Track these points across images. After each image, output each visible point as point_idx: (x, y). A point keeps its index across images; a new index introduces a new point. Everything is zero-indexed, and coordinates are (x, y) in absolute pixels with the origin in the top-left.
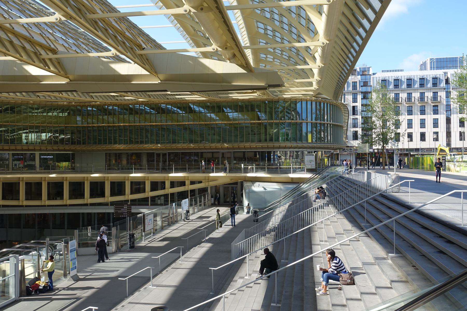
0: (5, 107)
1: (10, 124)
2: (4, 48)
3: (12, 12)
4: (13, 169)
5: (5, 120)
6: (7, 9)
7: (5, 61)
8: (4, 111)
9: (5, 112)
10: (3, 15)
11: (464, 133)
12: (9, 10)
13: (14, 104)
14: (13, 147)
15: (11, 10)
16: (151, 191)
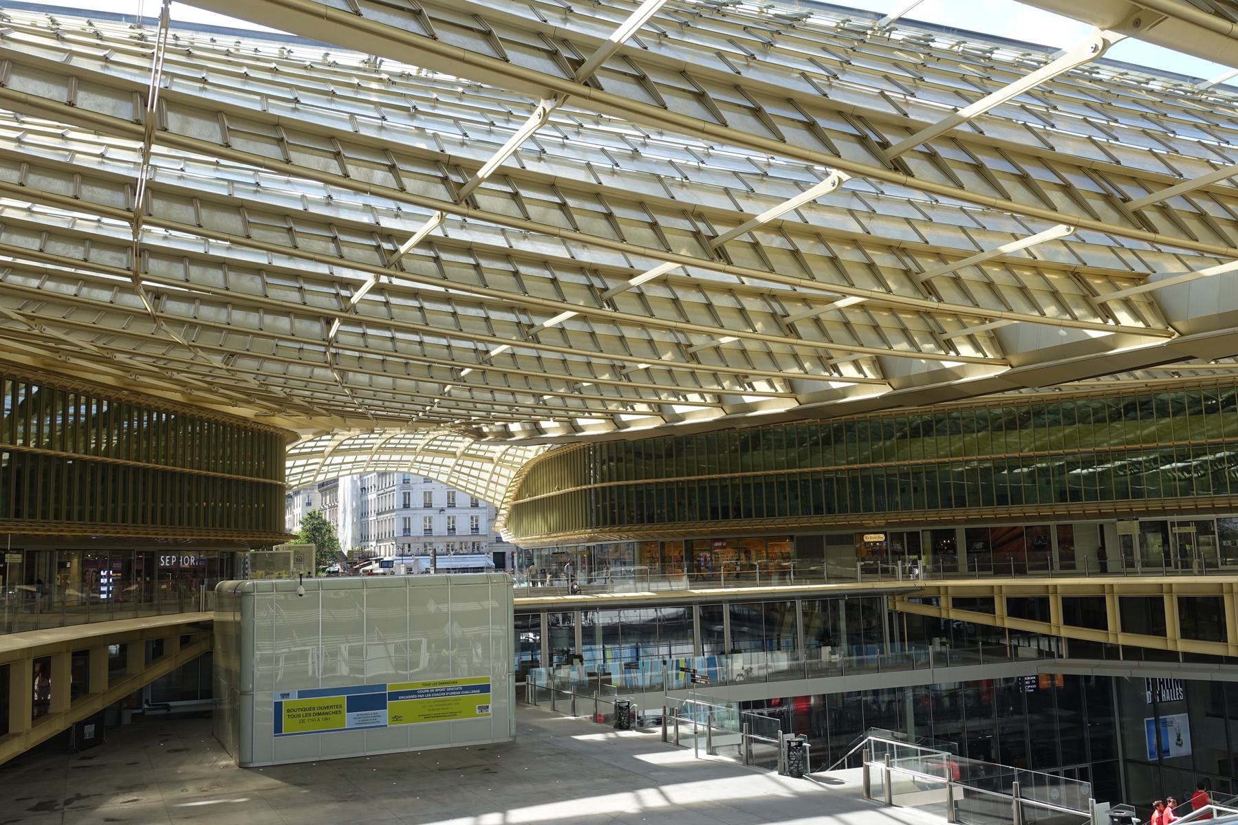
0: (1225, 395)
1: (1143, 446)
2: (1222, 243)
3: (1230, 146)
4: (1145, 565)
5: (1227, 429)
6: (1217, 144)
7: (1222, 275)
8: (1223, 408)
9: (1225, 409)
10: (1208, 161)
11: (409, 519)
12: (1223, 145)
13: (1215, 387)
14: (1138, 505)
15: (1228, 143)
16: (1105, 627)
